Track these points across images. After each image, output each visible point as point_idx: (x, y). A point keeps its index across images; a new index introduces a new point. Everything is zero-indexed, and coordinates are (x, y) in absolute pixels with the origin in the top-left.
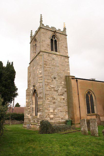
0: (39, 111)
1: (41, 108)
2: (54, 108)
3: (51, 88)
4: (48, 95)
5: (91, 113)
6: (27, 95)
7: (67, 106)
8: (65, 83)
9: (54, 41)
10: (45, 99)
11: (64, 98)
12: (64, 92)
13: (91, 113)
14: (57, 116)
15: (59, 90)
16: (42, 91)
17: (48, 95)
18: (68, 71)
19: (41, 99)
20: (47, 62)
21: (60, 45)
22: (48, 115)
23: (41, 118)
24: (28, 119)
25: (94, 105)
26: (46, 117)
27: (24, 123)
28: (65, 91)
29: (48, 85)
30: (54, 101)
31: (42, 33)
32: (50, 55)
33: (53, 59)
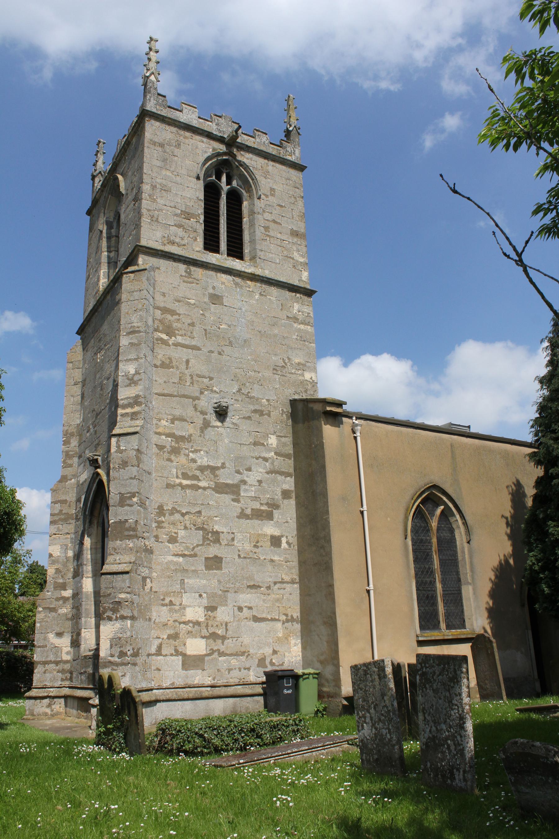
0: (109, 613)
1: (123, 596)
2: (212, 596)
3: (198, 473)
4: (173, 511)
5: (443, 625)
6: (56, 518)
7: (293, 582)
8: (285, 444)
9: (224, 197)
10: (157, 537)
11: (277, 533)
12: (279, 496)
13: (443, 625)
14: (230, 645)
15: (244, 482)
16: (136, 490)
17: (177, 516)
18: (308, 376)
19: (129, 537)
20: (173, 312)
21: (260, 220)
22: (174, 637)
23: (122, 654)
24: (57, 663)
25: (459, 580)
26: (159, 652)
27: (33, 693)
28: (286, 494)
29: (175, 451)
30: (213, 551)
31: (154, 143)
32: (198, 272)
33: (216, 299)
